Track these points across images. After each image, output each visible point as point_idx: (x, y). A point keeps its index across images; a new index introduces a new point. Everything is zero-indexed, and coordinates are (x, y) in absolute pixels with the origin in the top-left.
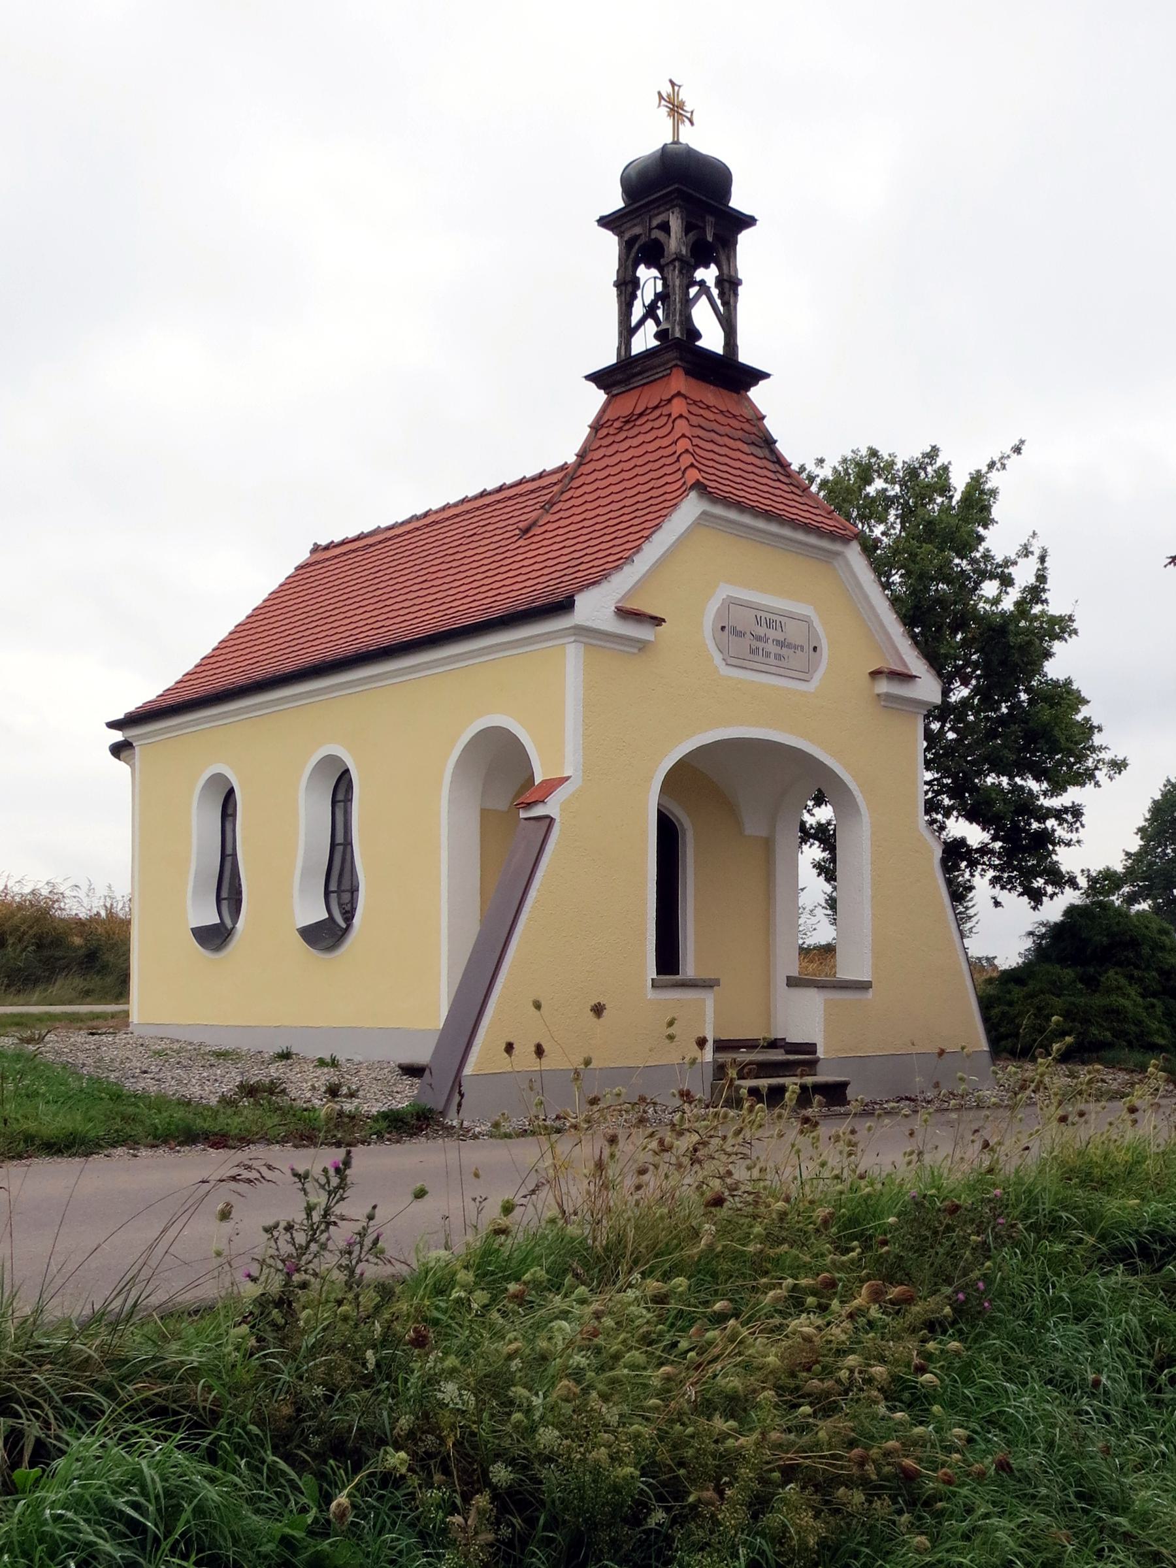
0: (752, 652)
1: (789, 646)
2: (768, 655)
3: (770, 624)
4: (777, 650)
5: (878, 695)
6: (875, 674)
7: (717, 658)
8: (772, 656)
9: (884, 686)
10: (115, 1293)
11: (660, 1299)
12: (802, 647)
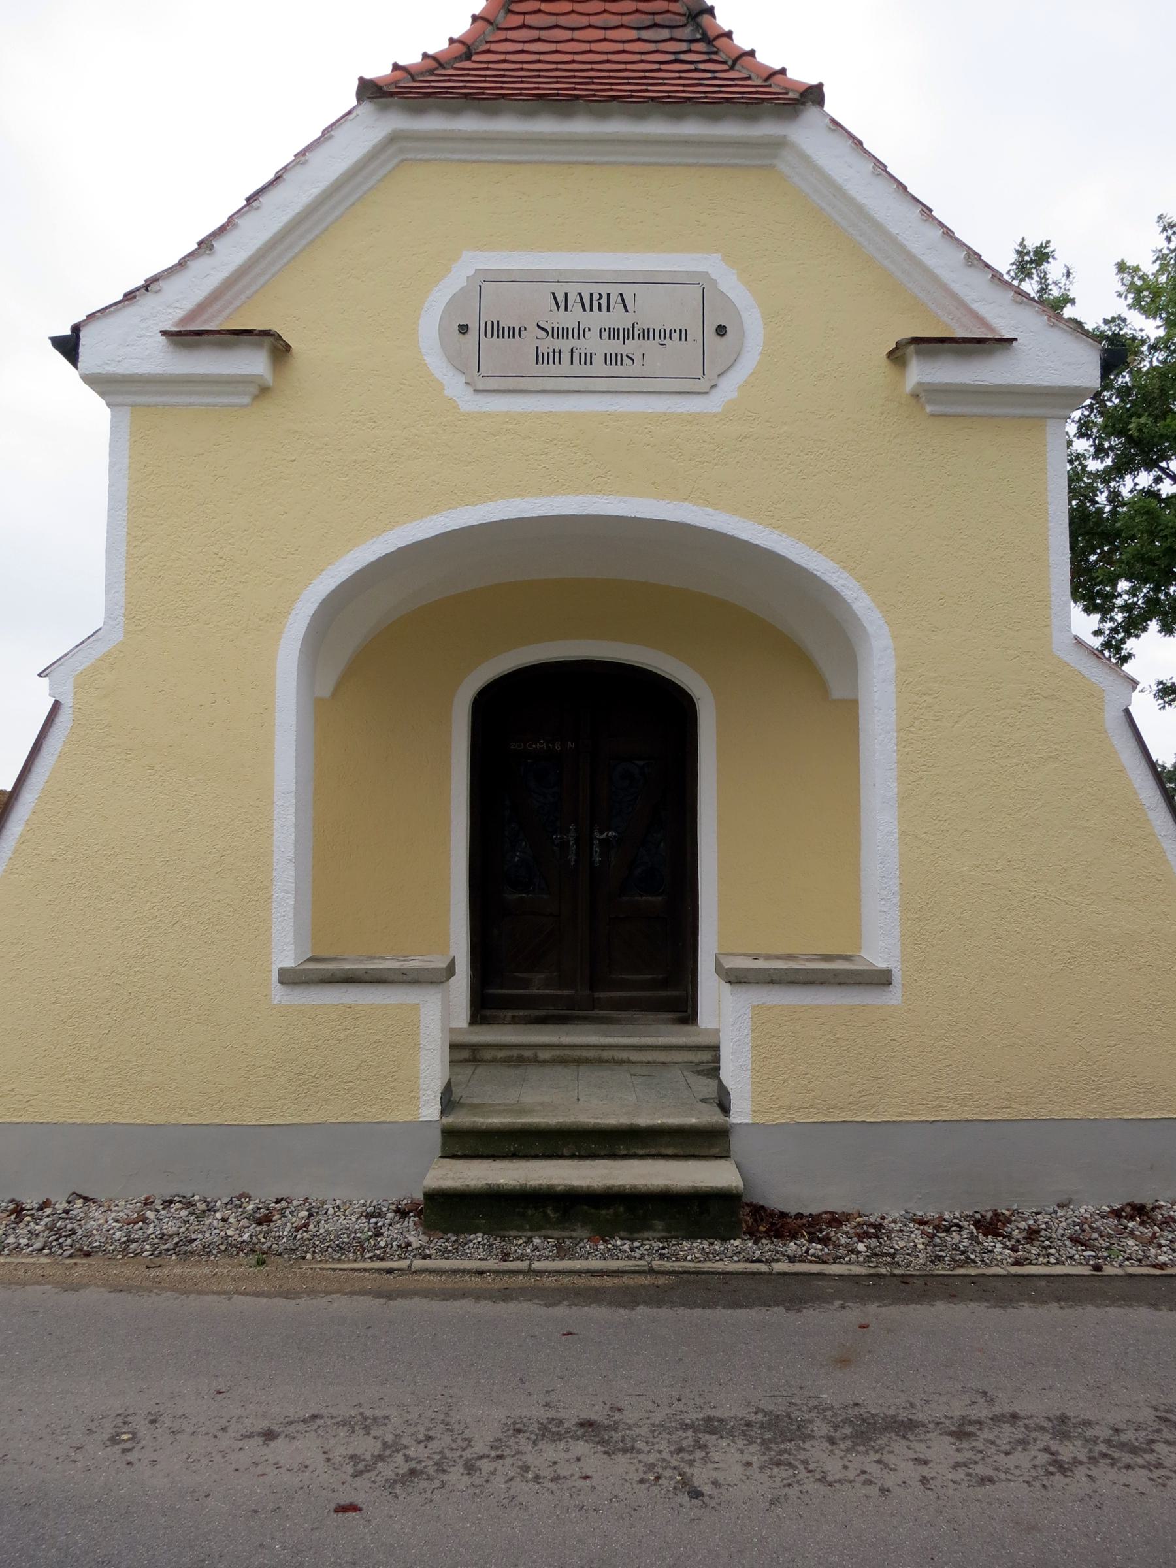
0: (539, 358)
1: (647, 334)
2: (586, 359)
3: (589, 304)
4: (616, 346)
5: (915, 396)
6: (897, 356)
7: (454, 385)
8: (598, 359)
9: (919, 372)
10: (731, 1256)
11: (979, 1429)
12: (684, 335)
